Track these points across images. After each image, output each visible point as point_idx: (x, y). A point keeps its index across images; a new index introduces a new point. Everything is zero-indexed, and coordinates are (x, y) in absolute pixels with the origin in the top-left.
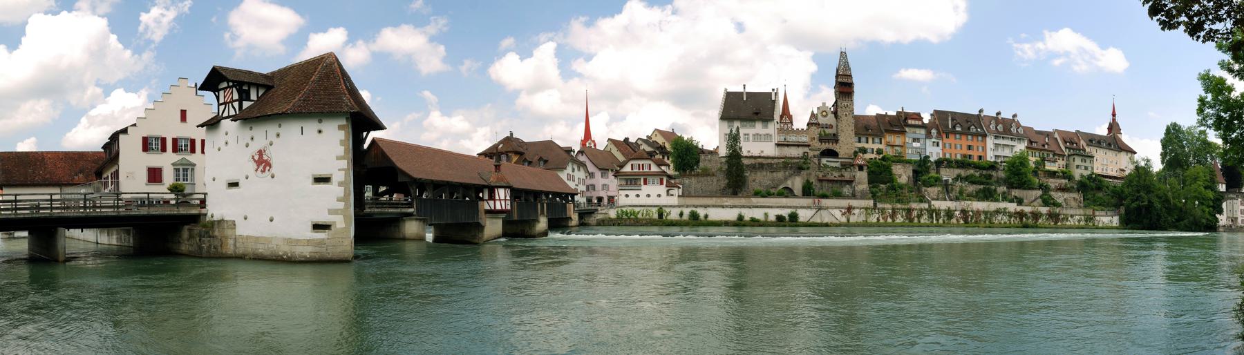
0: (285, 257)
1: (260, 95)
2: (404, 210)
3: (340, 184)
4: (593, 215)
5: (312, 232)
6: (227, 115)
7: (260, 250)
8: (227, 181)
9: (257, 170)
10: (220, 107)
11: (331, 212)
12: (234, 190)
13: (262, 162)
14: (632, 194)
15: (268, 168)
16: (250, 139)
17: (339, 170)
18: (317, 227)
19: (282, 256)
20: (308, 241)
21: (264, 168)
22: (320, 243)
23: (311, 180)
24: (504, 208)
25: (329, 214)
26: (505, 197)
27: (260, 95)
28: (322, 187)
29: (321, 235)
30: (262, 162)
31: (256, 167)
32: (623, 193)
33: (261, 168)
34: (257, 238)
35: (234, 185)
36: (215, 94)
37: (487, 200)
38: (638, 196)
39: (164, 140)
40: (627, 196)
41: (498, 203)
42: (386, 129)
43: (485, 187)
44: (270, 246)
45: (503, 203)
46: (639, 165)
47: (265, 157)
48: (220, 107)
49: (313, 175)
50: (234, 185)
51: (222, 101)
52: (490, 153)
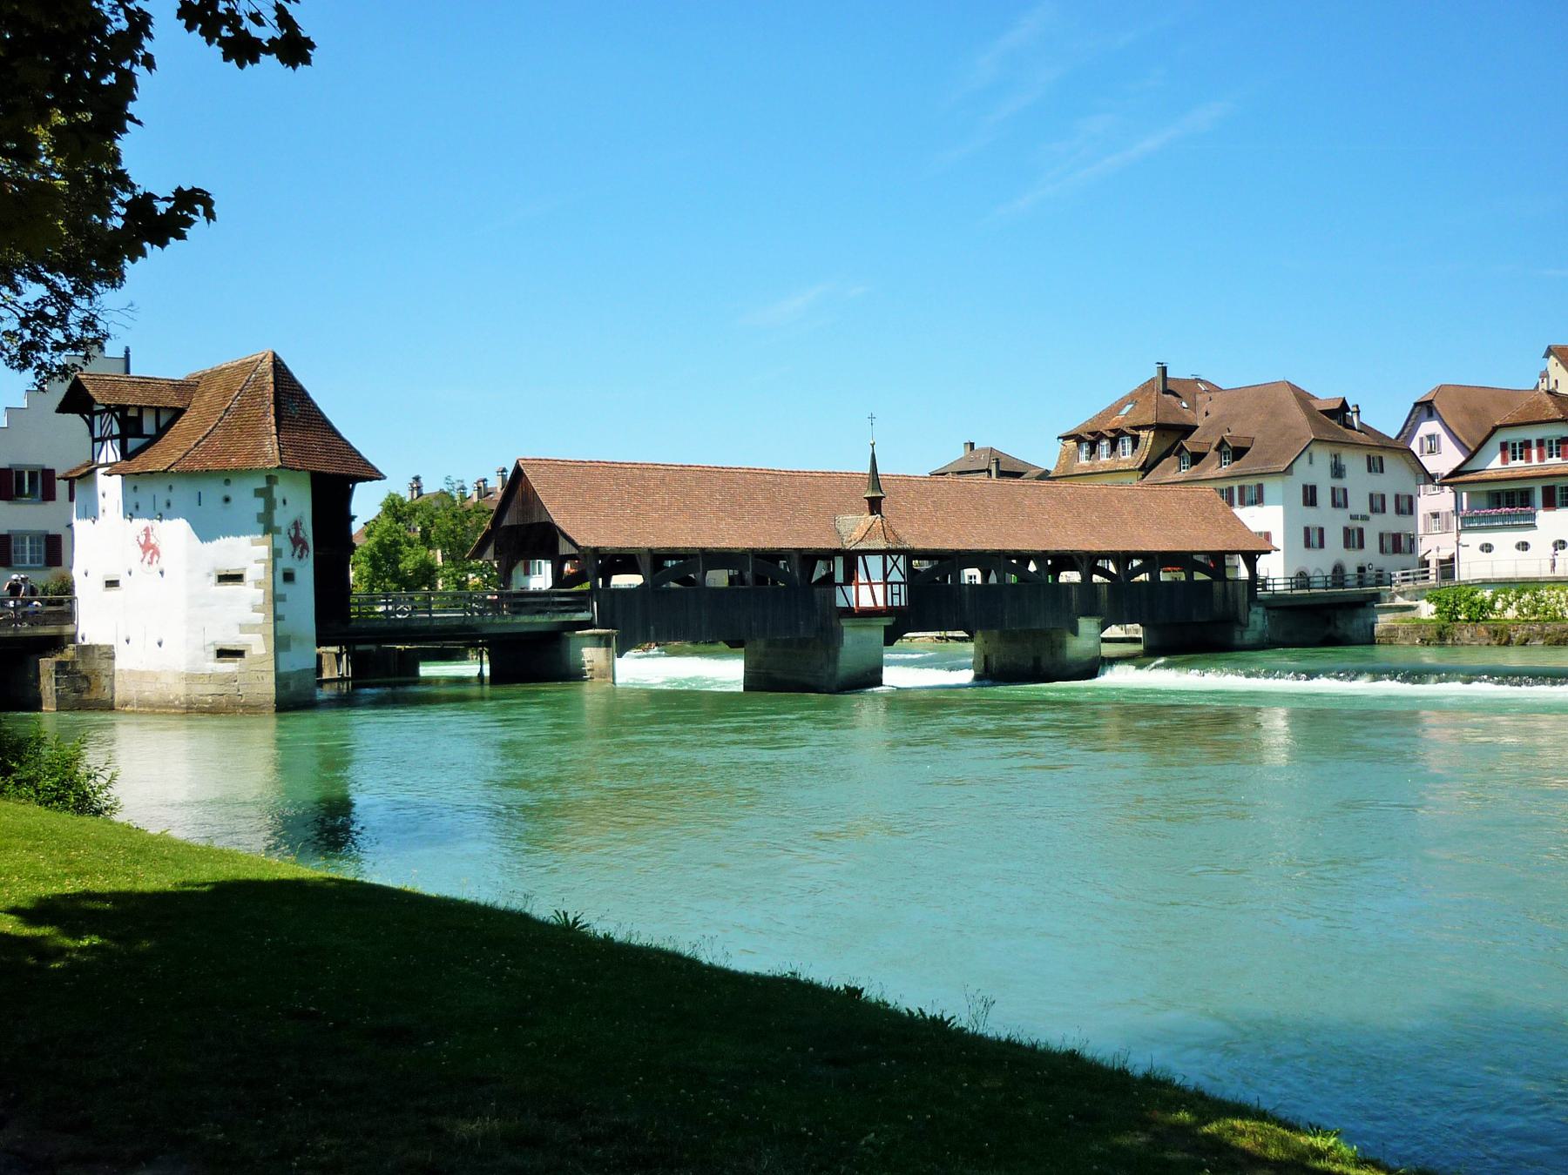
0: (177, 702)
1: (162, 425)
2: (566, 618)
3: (258, 584)
4: (1361, 611)
5: (215, 661)
6: (105, 462)
7: (146, 693)
8: (105, 576)
9: (142, 561)
10: (96, 444)
11: (243, 628)
12: (113, 592)
13: (149, 548)
14: (1504, 540)
15: (156, 558)
16: (134, 508)
17: (256, 562)
18: (222, 653)
19: (172, 702)
20: (210, 676)
21: (152, 558)
22: (230, 679)
23: (214, 579)
24: (881, 603)
25: (241, 632)
26: (886, 576)
27: (162, 425)
28: (230, 588)
29: (229, 666)
30: (149, 548)
31: (142, 556)
32: (1475, 539)
33: (148, 556)
34: (142, 673)
35: (112, 584)
36: (85, 419)
37: (841, 585)
38: (1524, 546)
39: (48, 475)
40: (1487, 548)
41: (864, 591)
42: (385, 478)
43: (838, 552)
44: (158, 686)
45: (879, 590)
46: (1231, 490)
47: (153, 541)
48: (96, 444)
49: (215, 570)
50: (112, 584)
51: (97, 435)
52: (1092, 434)
